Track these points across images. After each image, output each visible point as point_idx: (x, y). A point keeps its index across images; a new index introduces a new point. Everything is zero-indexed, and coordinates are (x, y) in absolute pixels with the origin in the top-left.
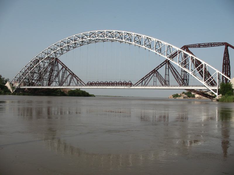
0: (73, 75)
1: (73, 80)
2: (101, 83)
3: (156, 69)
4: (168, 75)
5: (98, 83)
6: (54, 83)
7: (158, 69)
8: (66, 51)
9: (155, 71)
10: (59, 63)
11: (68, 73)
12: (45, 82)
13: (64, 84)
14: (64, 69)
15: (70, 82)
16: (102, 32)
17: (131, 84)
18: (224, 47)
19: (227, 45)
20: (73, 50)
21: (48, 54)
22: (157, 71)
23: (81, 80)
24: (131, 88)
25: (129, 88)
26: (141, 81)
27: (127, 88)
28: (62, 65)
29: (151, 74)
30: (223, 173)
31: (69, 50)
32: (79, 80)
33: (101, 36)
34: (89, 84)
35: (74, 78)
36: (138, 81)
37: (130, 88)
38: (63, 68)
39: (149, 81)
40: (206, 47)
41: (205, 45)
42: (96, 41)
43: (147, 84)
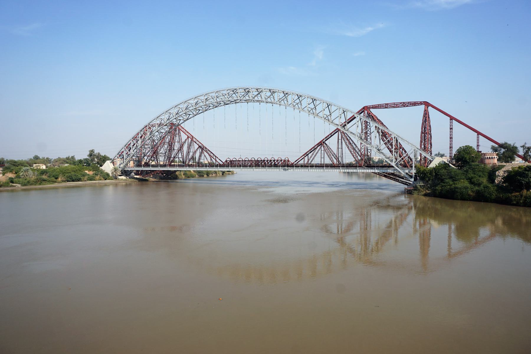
1: (204, 154)
14: (190, 139)
35: (205, 153)
41: (395, 106)
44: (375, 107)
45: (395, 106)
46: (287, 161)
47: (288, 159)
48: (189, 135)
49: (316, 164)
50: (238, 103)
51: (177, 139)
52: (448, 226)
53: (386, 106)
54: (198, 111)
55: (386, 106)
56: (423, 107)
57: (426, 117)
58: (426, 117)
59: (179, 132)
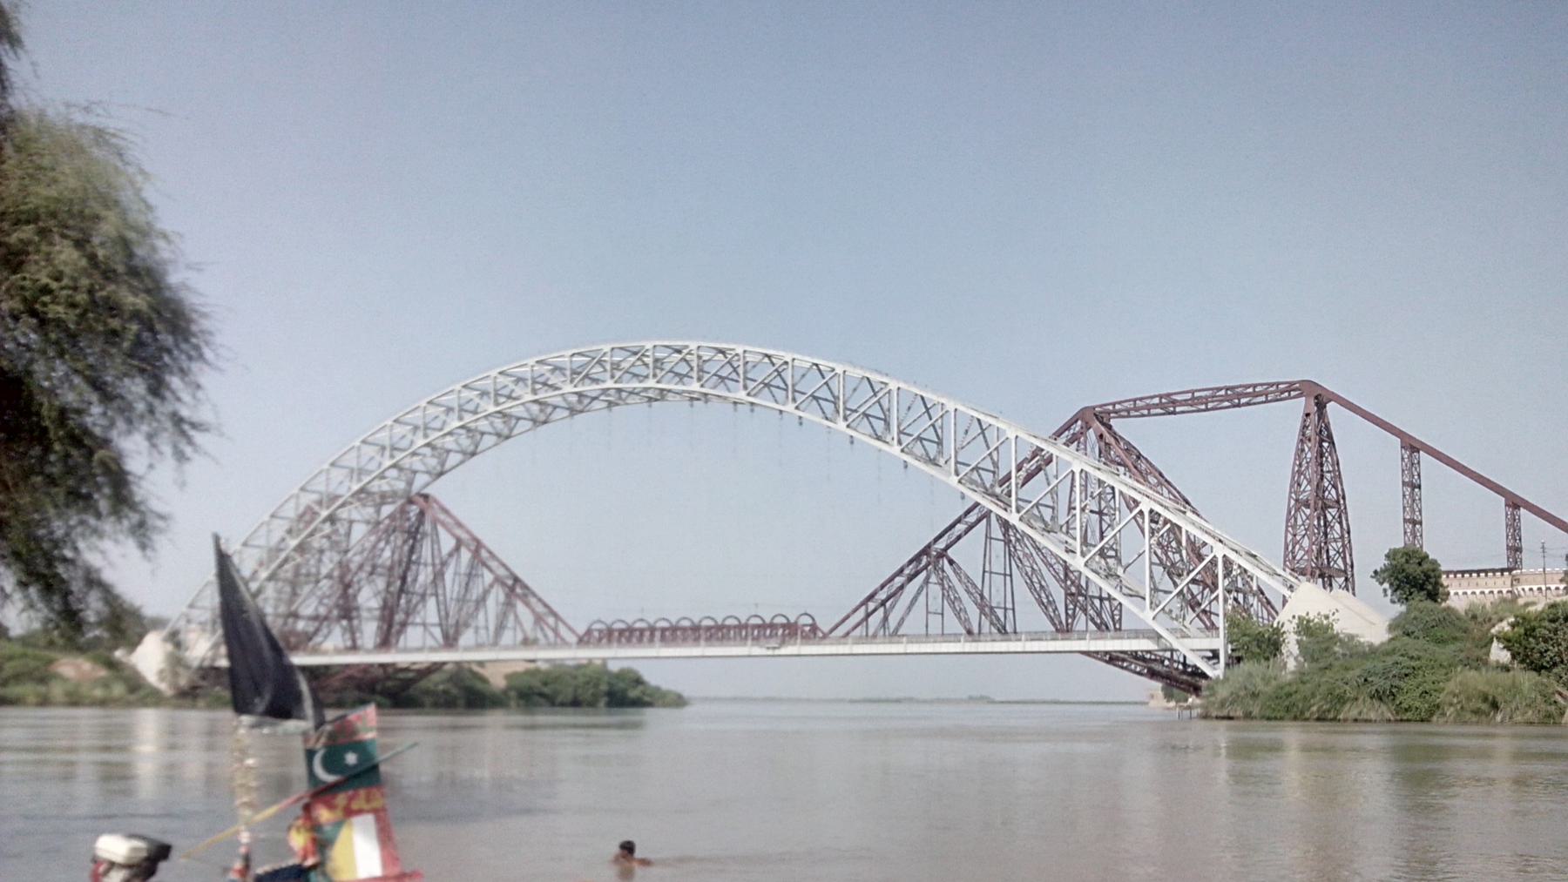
0: (515, 588)
1: (516, 617)
2: (729, 628)
3: (941, 545)
4: (1011, 575)
5: (758, 626)
6: (413, 636)
7: (948, 547)
8: (493, 439)
9: (930, 559)
10: (444, 524)
11: (488, 577)
12: (369, 631)
13: (467, 638)
14: (466, 555)
15: (500, 627)
16: (635, 350)
17: (813, 633)
18: (1299, 405)
19: (1321, 401)
20: (568, 420)
21: (461, 410)
22: (942, 554)
23: (555, 615)
24: (784, 651)
25: (770, 652)
26: (861, 613)
27: (763, 651)
28: (454, 535)
29: (911, 578)
30: (528, 811)
31: (545, 422)
32: (546, 615)
33: (634, 370)
34: (596, 634)
35: (520, 607)
36: (849, 610)
37: (777, 652)
38: (457, 549)
39: (848, 617)
40: (1207, 410)
41: (1201, 402)
42: (616, 399)
43: (897, 629)
44: (1137, 408)
45: (1201, 402)
46: (807, 629)
47: (813, 619)
48: (464, 536)
49: (1062, 639)
50: (581, 412)
51: (426, 551)
52: (369, 819)
53: (1168, 405)
54: (1128, 414)
55: (1168, 405)
56: (1299, 405)
57: (1320, 438)
58: (1320, 438)
59: (435, 528)
